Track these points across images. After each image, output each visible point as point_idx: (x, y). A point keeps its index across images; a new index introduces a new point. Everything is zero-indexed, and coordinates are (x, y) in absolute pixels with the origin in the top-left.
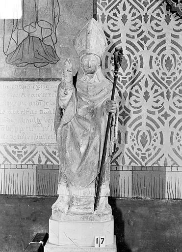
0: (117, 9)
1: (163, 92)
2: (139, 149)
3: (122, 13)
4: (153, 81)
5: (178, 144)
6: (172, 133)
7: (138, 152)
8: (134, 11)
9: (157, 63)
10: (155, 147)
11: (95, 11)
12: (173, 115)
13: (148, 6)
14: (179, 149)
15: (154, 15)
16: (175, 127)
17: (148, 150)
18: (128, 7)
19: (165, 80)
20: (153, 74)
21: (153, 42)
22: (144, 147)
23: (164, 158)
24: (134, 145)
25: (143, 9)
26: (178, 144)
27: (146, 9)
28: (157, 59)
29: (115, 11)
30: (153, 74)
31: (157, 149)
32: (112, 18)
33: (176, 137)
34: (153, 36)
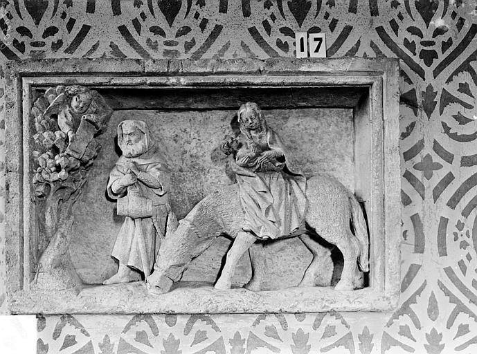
0: (413, 316)
1: (414, 90)
2: (157, 30)
3: (428, 325)
4: (454, 300)
5: (462, 255)
6: (444, 222)
7: (154, 38)
8: (462, 318)
9: (460, 239)
10: (205, 21)
11: (117, 109)
12: (447, 168)
13: (436, 62)
14: (464, 269)
15: (453, 89)
16: (453, 203)
17: (187, 30)
18: (446, 308)
19: (418, 51)
20: (449, 271)
21: (449, 178)
22: (37, 23)
23: (426, 294)
24: (140, 19)
25: (421, 73)
26: (462, 255)
27: (429, 71)
28: (460, 226)
29: (405, 320)
30: (449, 271)
31: (210, 27)
32: (396, 343)
33: (455, 234)
34: (449, 158)
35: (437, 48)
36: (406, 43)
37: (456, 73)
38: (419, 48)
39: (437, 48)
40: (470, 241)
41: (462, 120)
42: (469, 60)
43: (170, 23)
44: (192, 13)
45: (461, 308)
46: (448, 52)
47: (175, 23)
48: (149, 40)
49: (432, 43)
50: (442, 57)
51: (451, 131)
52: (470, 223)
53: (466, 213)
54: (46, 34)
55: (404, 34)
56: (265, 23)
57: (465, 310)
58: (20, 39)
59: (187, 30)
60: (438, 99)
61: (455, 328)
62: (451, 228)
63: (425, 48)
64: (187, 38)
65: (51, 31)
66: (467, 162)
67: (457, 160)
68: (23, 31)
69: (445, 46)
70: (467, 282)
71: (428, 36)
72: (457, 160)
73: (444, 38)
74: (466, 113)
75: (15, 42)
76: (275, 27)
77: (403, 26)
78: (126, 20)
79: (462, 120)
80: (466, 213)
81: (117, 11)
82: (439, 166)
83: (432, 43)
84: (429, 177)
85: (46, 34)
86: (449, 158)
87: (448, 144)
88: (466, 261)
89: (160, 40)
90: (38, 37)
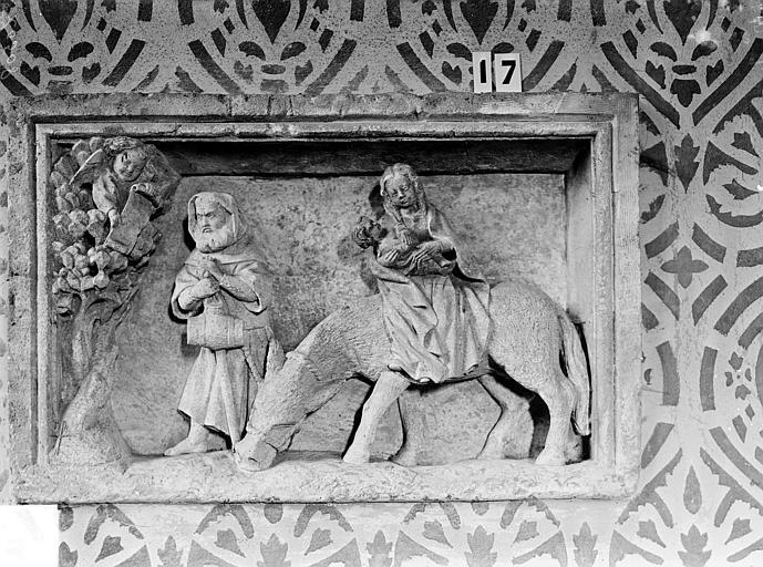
0: (660, 506)
1: (661, 145)
2: (250, 49)
3: (685, 521)
4: (726, 480)
5: (739, 408)
6: (710, 355)
7: (246, 60)
8: (740, 510)
9: (737, 383)
11: (187, 175)
12: (714, 269)
13: (698, 100)
14: (742, 431)
15: (724, 143)
16: (724, 325)
17: (299, 48)
18: (713, 493)
19: (668, 82)
20: (718, 434)
21: (719, 285)
23: (681, 471)
24: (224, 30)
25: (674, 118)
26: (739, 408)
27: (686, 114)
28: (736, 362)
29: (648, 512)
30: (718, 434)
32: (634, 549)
33: (728, 375)
34: (718, 253)
35: (699, 76)
36: (650, 68)
37: (729, 117)
38: (670, 77)
39: (699, 76)
40: (751, 386)
41: (738, 192)
42: (750, 97)
43: (273, 36)
44: (308, 21)
45: (737, 494)
46: (716, 84)
47: (280, 36)
48: (238, 64)
49: (691, 69)
50: (707, 91)
51: (722, 210)
52: (752, 357)
53: (745, 342)
54: (74, 55)
55: (646, 55)
56: (424, 37)
57: (745, 497)
58: (33, 62)
59: (299, 48)
60: (700, 158)
61: (728, 526)
62: (722, 366)
63: (680, 77)
64: (300, 61)
65: (82, 50)
66: (747, 259)
67: (731, 257)
68: (37, 49)
69: (712, 73)
70: (747, 451)
71: (684, 58)
72: (731, 257)
73: (711, 61)
74: (746, 181)
75: (24, 67)
76: (440, 43)
77: (645, 42)
78: (201, 32)
79: (738, 192)
80: (745, 342)
81: (187, 17)
82: (702, 267)
83: (691, 69)
84: (686, 283)
85: (74, 55)
86: (718, 253)
87: (716, 231)
88: (745, 419)
89: (256, 63)
90: (61, 60)
